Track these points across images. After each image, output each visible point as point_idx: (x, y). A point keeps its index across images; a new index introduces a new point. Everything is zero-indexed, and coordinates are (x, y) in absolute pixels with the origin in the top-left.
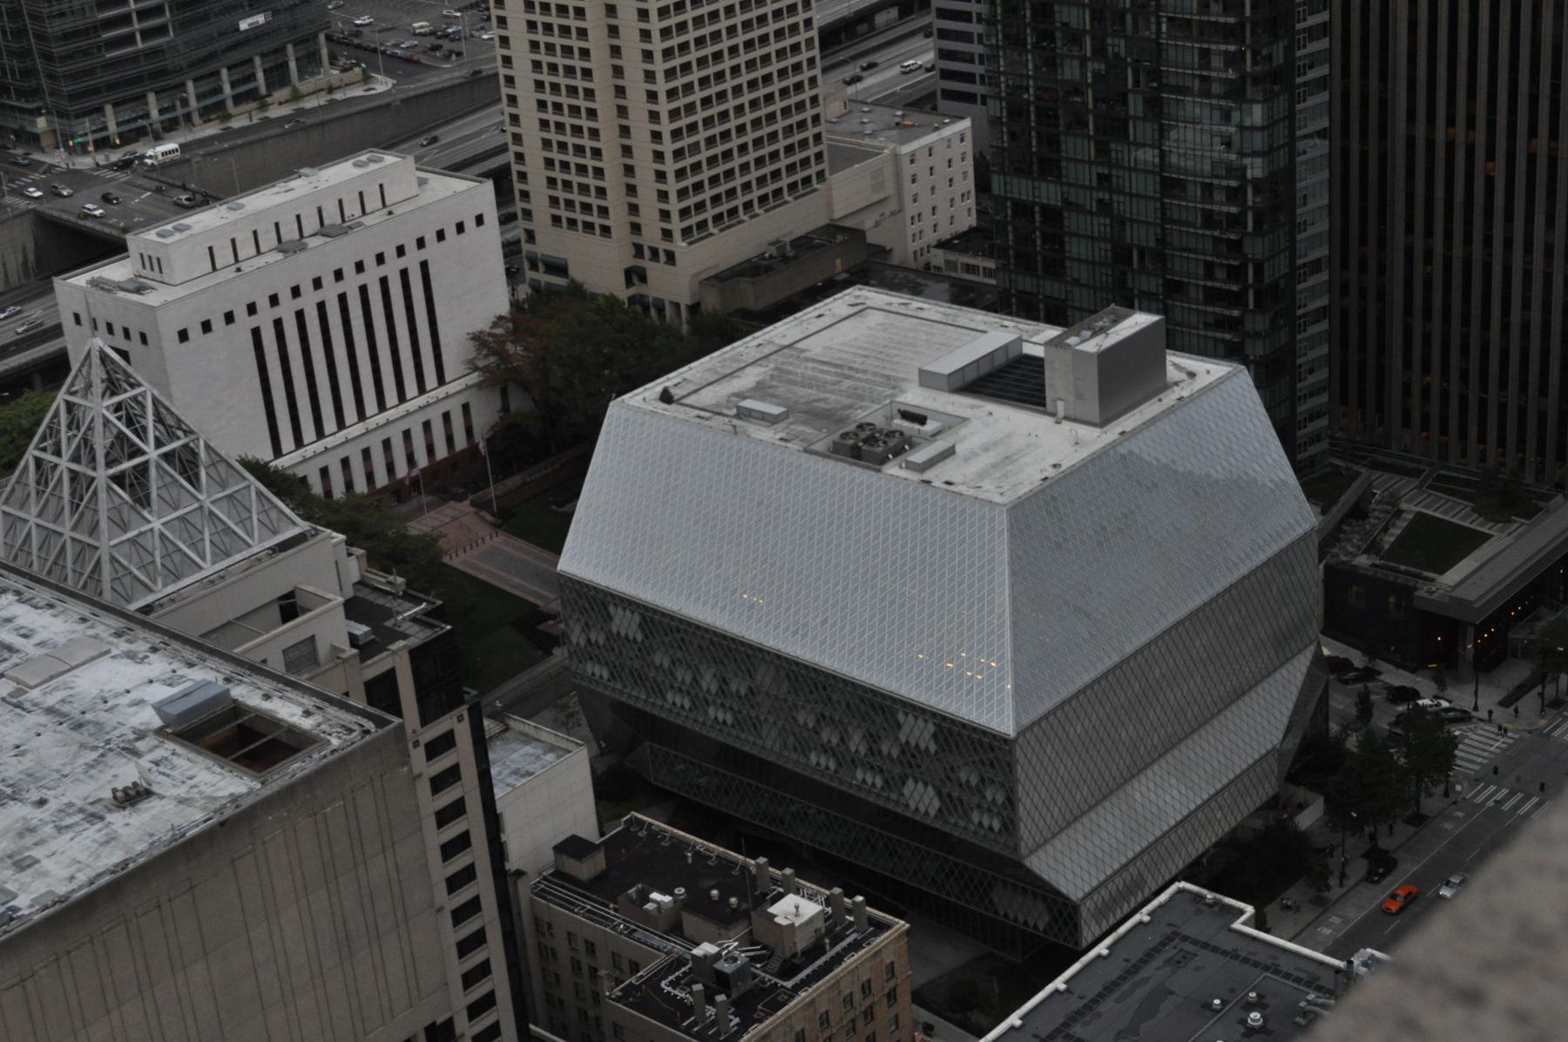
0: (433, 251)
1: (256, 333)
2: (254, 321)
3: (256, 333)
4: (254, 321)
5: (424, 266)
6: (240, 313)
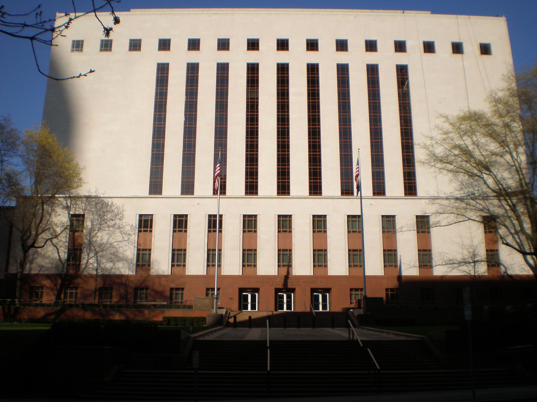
0: (413, 58)
1: (163, 70)
2: (164, 57)
3: (163, 70)
4: (164, 57)
5: (402, 72)
6: (150, 45)
